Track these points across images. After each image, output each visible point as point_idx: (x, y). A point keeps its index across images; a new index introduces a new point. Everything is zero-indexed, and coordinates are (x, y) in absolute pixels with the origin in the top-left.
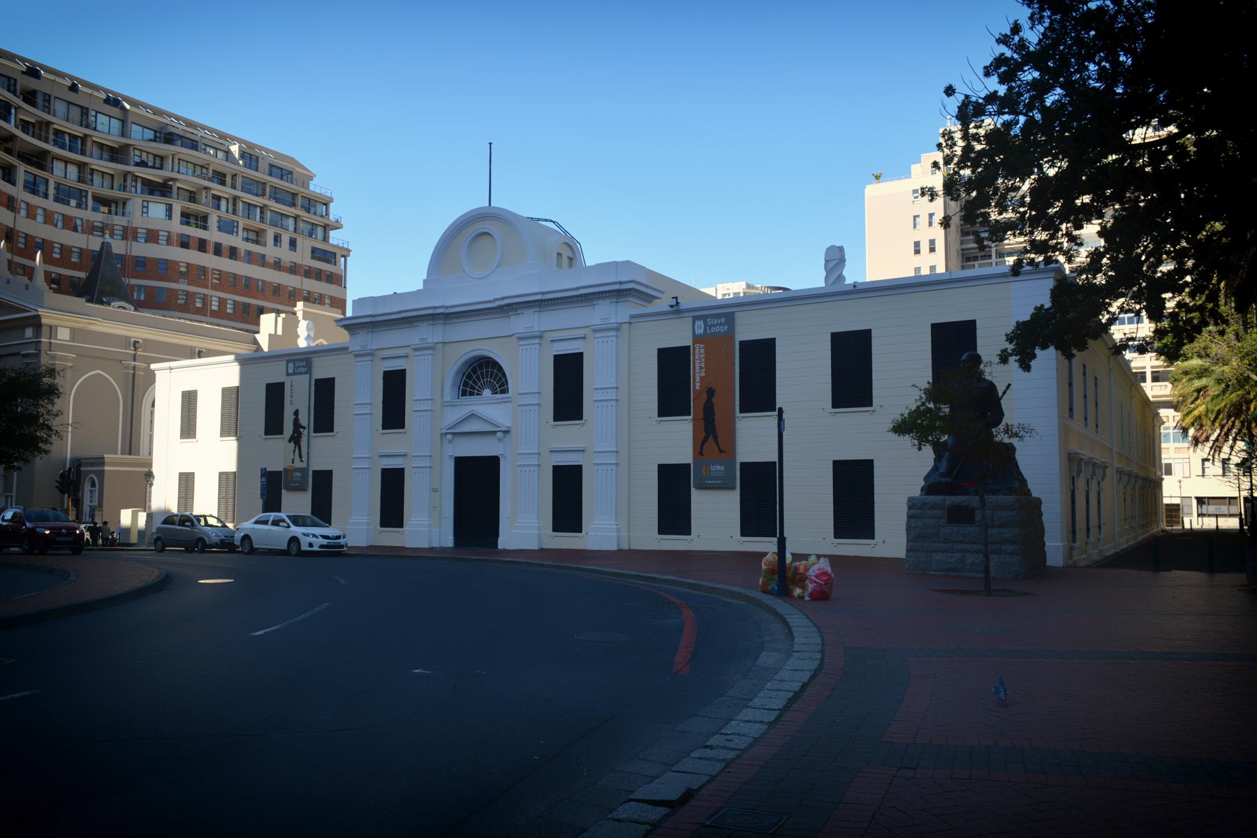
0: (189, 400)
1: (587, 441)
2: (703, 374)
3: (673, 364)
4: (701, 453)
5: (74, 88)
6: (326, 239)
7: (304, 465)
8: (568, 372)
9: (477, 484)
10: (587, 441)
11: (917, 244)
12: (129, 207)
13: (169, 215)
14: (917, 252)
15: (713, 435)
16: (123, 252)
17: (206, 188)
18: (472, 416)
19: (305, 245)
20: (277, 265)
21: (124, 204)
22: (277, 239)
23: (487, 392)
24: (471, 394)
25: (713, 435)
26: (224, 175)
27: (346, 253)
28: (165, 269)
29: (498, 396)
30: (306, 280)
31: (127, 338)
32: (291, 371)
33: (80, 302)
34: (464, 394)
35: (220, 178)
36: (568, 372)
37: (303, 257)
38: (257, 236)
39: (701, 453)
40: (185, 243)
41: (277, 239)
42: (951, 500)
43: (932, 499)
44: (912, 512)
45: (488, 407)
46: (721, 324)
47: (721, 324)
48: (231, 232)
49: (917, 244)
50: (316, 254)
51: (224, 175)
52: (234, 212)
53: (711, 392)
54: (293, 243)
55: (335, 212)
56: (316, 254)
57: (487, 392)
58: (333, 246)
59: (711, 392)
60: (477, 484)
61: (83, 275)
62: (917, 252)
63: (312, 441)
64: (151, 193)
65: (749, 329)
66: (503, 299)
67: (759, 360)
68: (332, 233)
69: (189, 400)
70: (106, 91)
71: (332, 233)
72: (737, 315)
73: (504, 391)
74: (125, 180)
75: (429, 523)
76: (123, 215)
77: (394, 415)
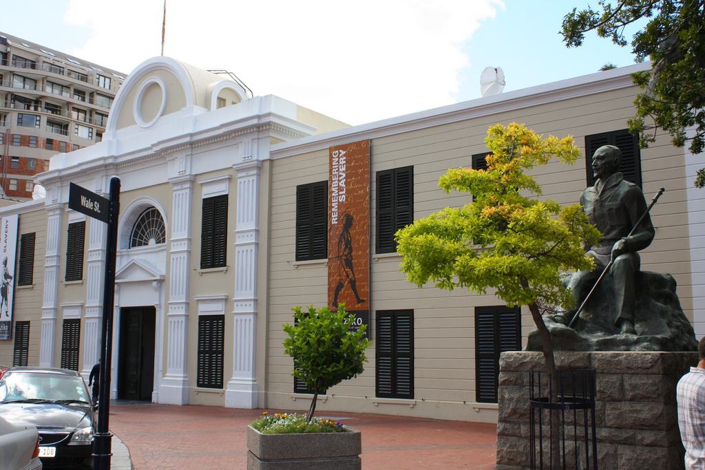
1: (237, 291)
3: (312, 199)
7: (9, 319)
10: (237, 291)
12: (8, 117)
21: (5, 116)
24: (140, 244)
26: (84, 93)
34: (134, 245)
51: (84, 93)
57: (152, 241)
63: (18, 294)
65: (385, 161)
66: (160, 143)
67: (396, 192)
72: (375, 143)
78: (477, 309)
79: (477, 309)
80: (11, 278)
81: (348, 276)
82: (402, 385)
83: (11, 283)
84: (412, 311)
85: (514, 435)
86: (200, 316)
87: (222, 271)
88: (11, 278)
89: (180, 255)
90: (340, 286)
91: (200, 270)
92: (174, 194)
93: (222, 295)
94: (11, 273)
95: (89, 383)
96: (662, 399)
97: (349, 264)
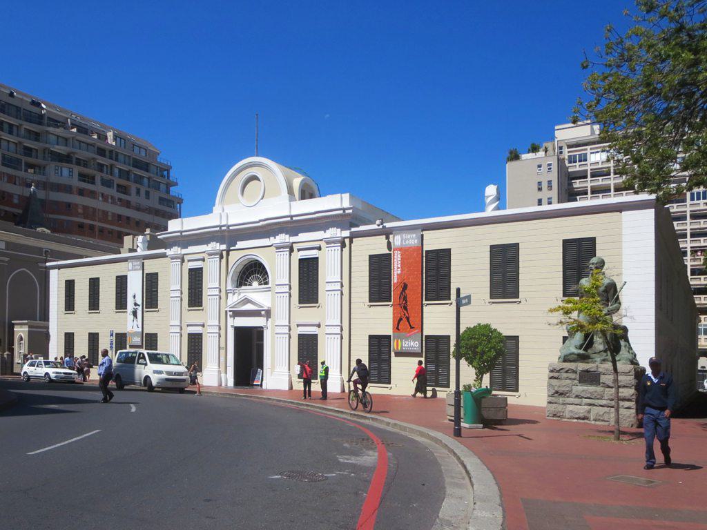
0: (70, 286)
1: (326, 315)
2: (399, 272)
4: (397, 328)
5: (11, 95)
6: (168, 191)
8: (309, 270)
9: (249, 349)
11: (540, 183)
12: (47, 168)
13: (71, 175)
14: (540, 189)
15: (407, 319)
16: (44, 198)
17: (93, 159)
18: (247, 301)
19: (155, 195)
20: (138, 209)
21: (44, 168)
22: (138, 192)
23: (255, 284)
25: (407, 319)
27: (180, 201)
28: (69, 208)
29: (263, 286)
30: (156, 218)
31: (41, 249)
32: (130, 268)
33: (11, 225)
35: (101, 152)
36: (309, 270)
37: (153, 202)
38: (123, 189)
39: (397, 328)
40: (81, 192)
41: (138, 192)
42: (582, 366)
43: (567, 365)
44: (552, 374)
45: (255, 294)
46: (412, 239)
47: (412, 239)
48: (109, 187)
49: (540, 183)
50: (161, 200)
52: (111, 174)
53: (405, 287)
54: (147, 194)
55: (173, 175)
56: (161, 200)
57: (255, 284)
58: (172, 196)
59: (405, 287)
60: (249, 349)
61: (20, 211)
62: (540, 189)
64: (61, 161)
68: (172, 189)
69: (70, 286)
70: (30, 97)
71: (172, 189)
73: (266, 283)
74: (44, 153)
75: (217, 373)
76: (44, 174)
77: (195, 298)
78: (369, 336)
79: (369, 336)
80: (139, 305)
81: (405, 315)
82: (67, 335)
83: (140, 308)
84: (518, 337)
85: (556, 403)
86: (299, 335)
87: (447, 304)
88: (139, 305)
89: (284, 294)
90: (400, 320)
91: (188, 308)
92: (56, 281)
93: (200, 322)
94: (140, 302)
95: (347, 380)
96: (633, 387)
97: (405, 308)
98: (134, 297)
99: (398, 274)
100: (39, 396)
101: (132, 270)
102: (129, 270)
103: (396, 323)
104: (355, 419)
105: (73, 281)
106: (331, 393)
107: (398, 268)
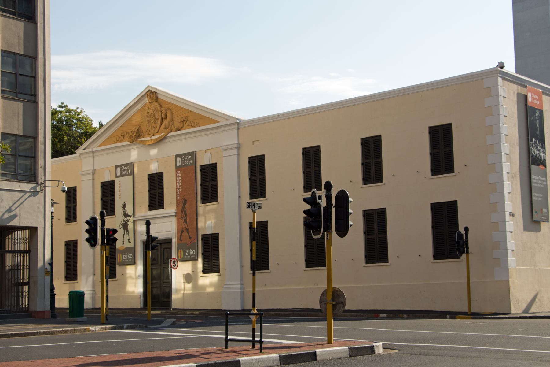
32: (118, 174)
46: (189, 160)
88: (130, 216)
90: (182, 231)
97: (185, 221)
98: (124, 207)
99: (180, 192)
100: (9, 14)
101: (121, 176)
102: (117, 177)
103: (180, 235)
104: (183, 351)
105: (261, 159)
106: (126, 268)
107: (180, 186)
